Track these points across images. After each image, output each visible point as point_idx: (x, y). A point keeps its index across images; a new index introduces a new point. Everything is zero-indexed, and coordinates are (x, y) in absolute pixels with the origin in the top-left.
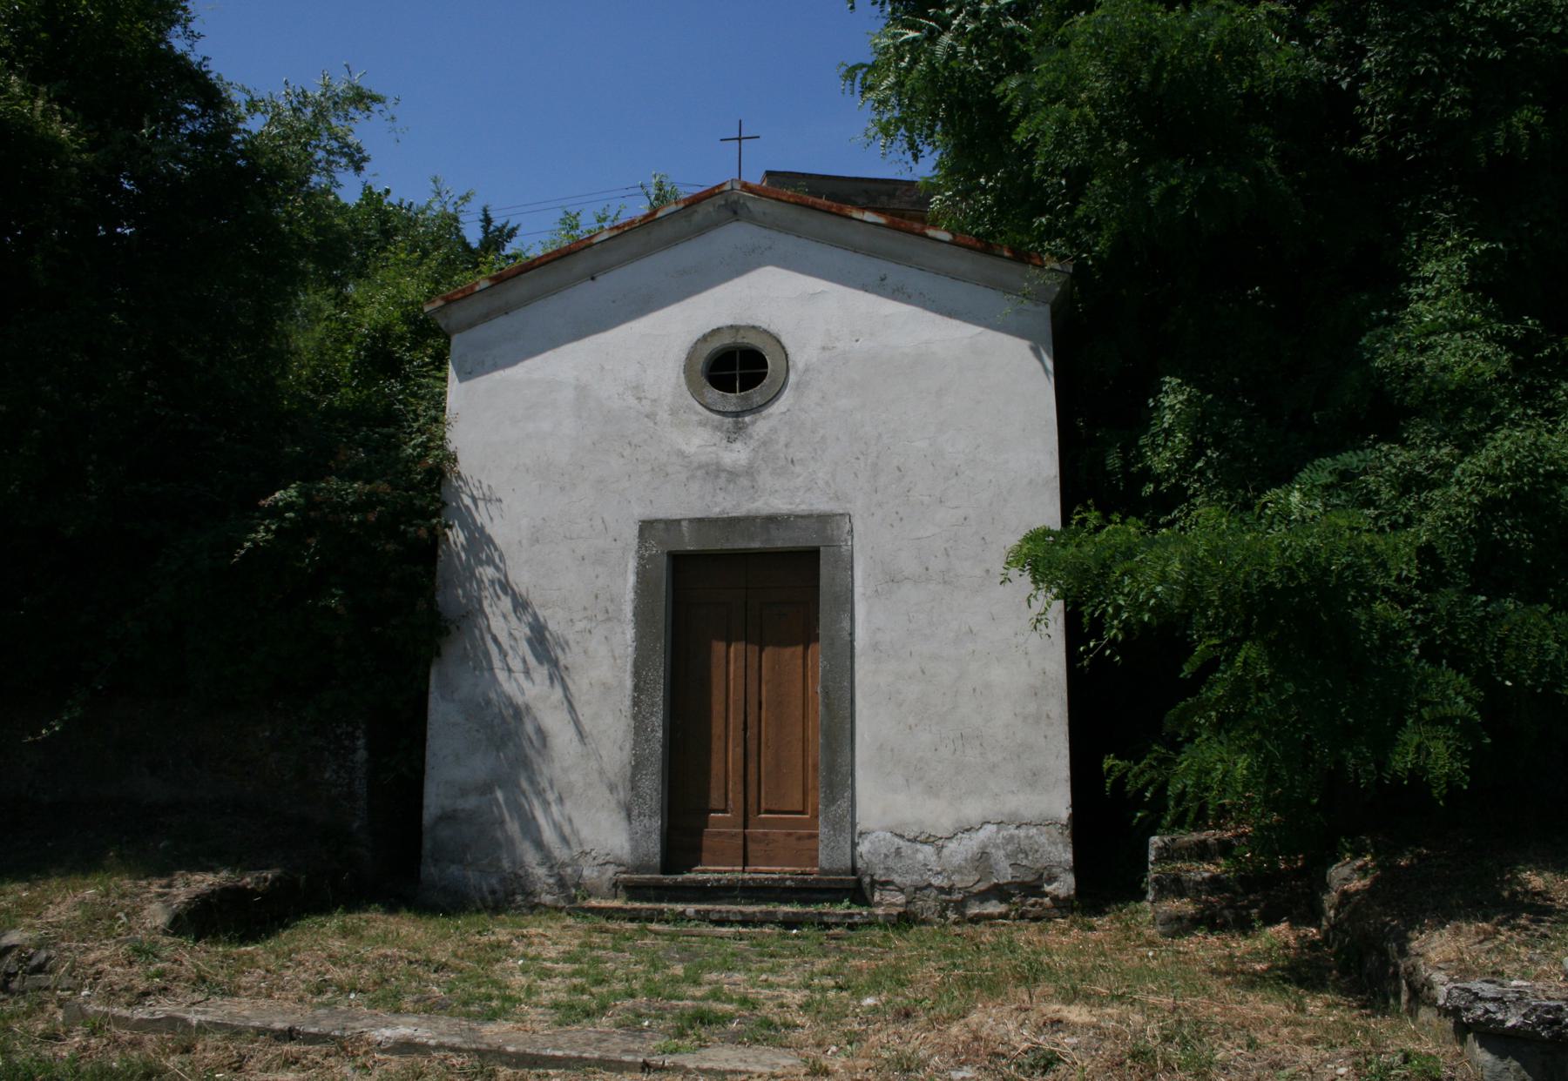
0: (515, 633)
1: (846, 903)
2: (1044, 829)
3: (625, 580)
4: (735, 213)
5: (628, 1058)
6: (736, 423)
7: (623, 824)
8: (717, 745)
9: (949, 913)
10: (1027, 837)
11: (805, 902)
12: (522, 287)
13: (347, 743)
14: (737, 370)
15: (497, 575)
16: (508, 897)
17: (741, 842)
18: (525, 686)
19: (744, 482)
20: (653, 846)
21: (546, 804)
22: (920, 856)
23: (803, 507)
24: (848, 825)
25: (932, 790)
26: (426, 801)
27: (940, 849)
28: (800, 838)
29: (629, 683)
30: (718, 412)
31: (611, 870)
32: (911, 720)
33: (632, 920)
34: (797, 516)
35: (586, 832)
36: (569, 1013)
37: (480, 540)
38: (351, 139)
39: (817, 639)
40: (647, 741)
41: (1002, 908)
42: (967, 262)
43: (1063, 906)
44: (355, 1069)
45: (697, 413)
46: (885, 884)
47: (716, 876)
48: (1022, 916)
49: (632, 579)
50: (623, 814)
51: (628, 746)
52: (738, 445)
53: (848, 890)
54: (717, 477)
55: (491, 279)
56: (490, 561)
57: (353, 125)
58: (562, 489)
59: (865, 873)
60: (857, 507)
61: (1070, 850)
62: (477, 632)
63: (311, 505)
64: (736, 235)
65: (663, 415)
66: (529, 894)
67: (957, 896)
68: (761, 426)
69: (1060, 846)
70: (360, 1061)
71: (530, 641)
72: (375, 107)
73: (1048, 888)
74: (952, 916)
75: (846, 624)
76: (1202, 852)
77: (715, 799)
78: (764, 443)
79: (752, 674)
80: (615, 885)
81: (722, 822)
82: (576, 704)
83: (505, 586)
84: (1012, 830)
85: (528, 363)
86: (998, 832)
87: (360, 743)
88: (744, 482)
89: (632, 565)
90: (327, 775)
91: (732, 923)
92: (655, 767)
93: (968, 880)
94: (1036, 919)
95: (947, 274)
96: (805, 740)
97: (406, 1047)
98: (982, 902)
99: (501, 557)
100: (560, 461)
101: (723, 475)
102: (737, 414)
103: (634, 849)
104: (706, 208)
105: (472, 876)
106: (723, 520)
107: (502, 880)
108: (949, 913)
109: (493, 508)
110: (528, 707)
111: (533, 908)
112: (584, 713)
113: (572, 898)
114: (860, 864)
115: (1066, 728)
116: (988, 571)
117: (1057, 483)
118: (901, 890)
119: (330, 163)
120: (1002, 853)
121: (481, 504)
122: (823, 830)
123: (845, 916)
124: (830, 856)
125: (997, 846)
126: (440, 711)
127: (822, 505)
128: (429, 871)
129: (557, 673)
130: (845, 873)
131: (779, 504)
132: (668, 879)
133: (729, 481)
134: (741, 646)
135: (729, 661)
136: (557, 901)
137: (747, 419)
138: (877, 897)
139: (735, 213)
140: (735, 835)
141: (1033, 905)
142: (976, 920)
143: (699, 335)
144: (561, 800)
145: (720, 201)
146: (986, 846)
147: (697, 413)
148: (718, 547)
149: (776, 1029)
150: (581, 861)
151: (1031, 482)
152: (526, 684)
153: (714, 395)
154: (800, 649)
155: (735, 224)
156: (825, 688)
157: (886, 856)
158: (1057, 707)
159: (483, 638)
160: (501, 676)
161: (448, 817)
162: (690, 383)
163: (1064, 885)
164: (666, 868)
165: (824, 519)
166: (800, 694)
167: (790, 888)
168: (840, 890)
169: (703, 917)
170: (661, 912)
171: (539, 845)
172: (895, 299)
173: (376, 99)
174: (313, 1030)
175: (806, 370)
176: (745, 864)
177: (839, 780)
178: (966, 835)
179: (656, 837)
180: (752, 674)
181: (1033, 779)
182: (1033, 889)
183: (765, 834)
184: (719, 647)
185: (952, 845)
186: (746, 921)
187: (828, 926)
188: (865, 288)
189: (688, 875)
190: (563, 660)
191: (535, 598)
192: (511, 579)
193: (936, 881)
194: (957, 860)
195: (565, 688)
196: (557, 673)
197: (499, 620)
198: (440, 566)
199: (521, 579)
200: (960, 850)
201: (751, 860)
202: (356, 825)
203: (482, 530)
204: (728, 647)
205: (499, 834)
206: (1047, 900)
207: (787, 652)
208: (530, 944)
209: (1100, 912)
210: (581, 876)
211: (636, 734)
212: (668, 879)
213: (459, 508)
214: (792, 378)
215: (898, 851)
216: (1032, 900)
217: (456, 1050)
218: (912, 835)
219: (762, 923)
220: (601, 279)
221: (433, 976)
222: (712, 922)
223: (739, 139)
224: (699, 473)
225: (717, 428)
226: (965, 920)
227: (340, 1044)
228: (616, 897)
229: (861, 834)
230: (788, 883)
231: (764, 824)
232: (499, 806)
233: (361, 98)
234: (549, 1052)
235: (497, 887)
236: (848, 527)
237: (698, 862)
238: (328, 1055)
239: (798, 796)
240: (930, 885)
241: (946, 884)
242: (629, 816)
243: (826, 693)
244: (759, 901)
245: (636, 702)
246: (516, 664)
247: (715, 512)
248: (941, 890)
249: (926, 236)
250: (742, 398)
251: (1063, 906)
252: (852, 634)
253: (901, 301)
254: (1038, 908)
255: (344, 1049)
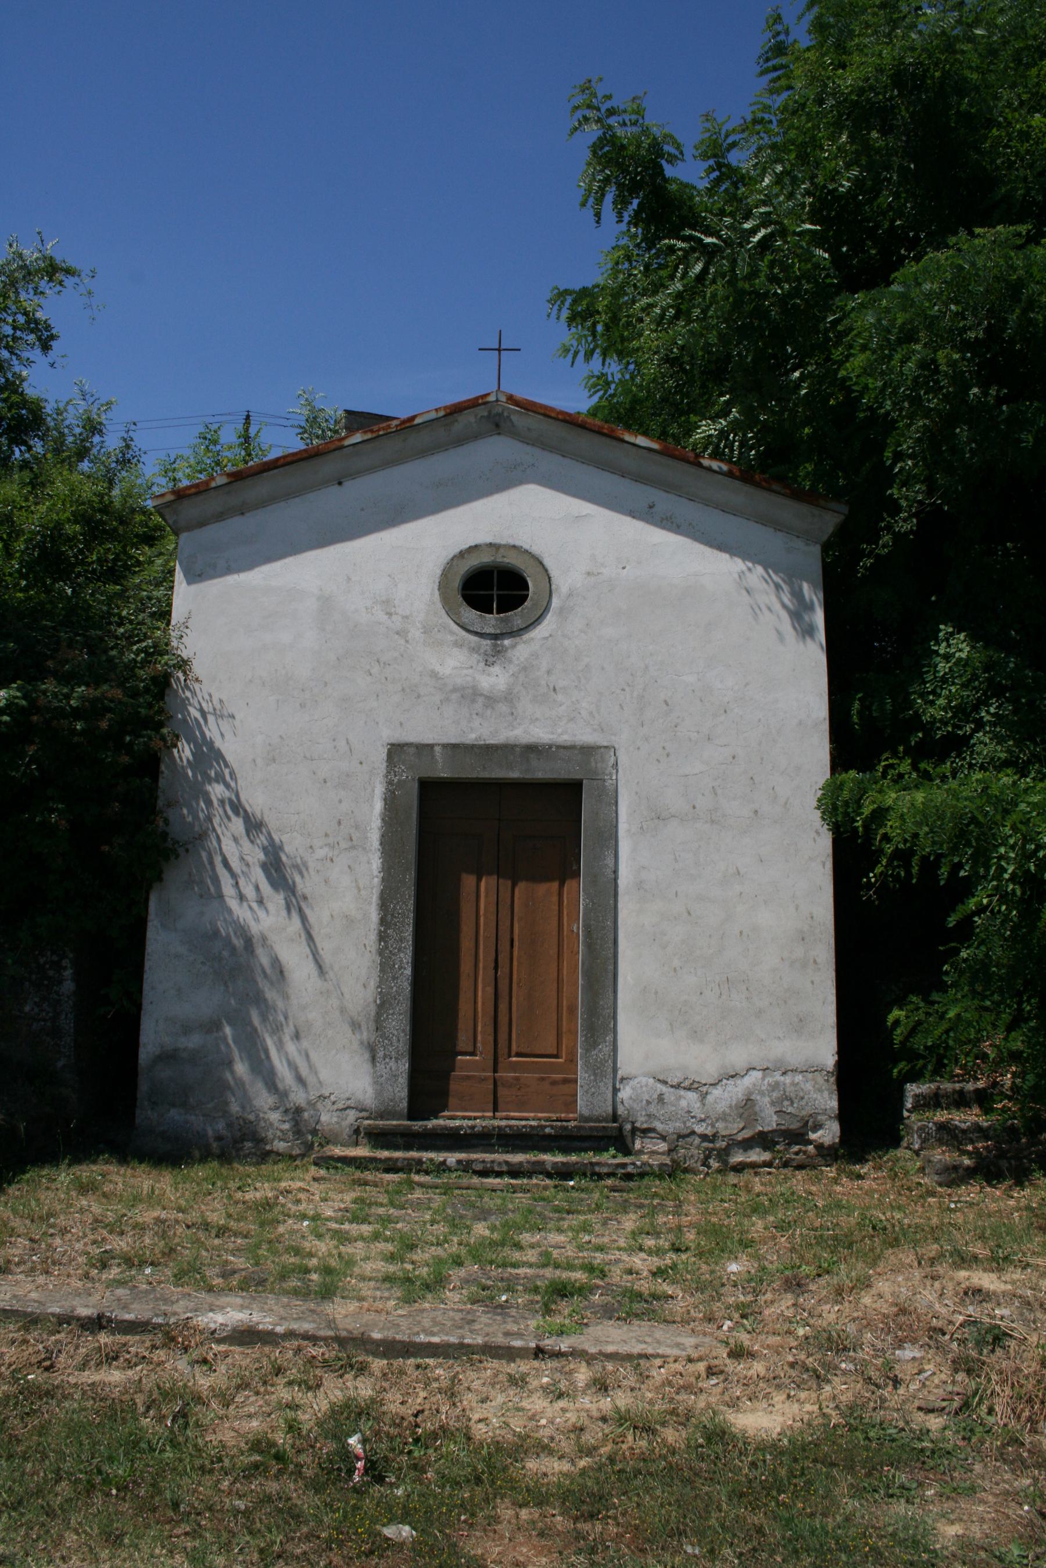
0: (248, 858)
1: (612, 1151)
2: (810, 1076)
3: (372, 806)
4: (497, 425)
5: (517, 1343)
6: (495, 646)
7: (367, 1067)
8: (465, 984)
9: (711, 1161)
10: (793, 1084)
11: (565, 1151)
12: (261, 487)
13: (51, 973)
14: (495, 590)
15: (227, 794)
16: (240, 1145)
17: (491, 1087)
18: (267, 920)
19: (503, 708)
20: (400, 1091)
21: (280, 1045)
22: (683, 1103)
23: (565, 737)
24: (608, 1069)
25: (696, 1035)
26: (143, 1039)
27: (704, 1096)
28: (554, 1083)
29: (374, 916)
30: (476, 634)
31: (352, 1115)
32: (676, 963)
33: (387, 1171)
34: (558, 747)
35: (324, 1074)
36: (414, 1289)
37: (209, 756)
38: (39, 315)
39: (577, 874)
40: (394, 978)
41: (766, 1156)
42: (739, 494)
43: (828, 1154)
44: (193, 1363)
45: (452, 633)
46: (645, 1131)
47: (470, 1123)
48: (786, 1165)
49: (378, 806)
50: (367, 1055)
51: (373, 984)
52: (496, 669)
53: (609, 1137)
54: (473, 701)
55: (229, 475)
56: (220, 778)
57: (42, 301)
58: (302, 706)
59: (626, 1120)
60: (622, 740)
61: (835, 1097)
62: (204, 854)
63: (34, 706)
64: (498, 448)
65: (416, 633)
66: (259, 1141)
67: (721, 1144)
68: (521, 650)
69: (826, 1094)
70: (195, 1354)
71: (264, 866)
72: (69, 281)
73: (813, 1136)
74: (715, 1164)
75: (610, 861)
76: (960, 1101)
77: (463, 1041)
78: (525, 669)
79: (504, 912)
80: (357, 1131)
81: (470, 1065)
82: (314, 934)
83: (237, 807)
84: (777, 1077)
85: (266, 569)
86: (763, 1079)
87: (68, 973)
88: (503, 708)
89: (379, 789)
90: (27, 1008)
91: (499, 1174)
92: (402, 1007)
93: (732, 1128)
94: (800, 1167)
95: (717, 507)
96: (559, 980)
97: (246, 1336)
98: (745, 1150)
99: (232, 774)
100: (302, 680)
101: (481, 700)
102: (495, 637)
103: (379, 1094)
104: (468, 418)
105: (195, 1120)
106: (480, 747)
107: (230, 1125)
108: (711, 1161)
109: (225, 725)
110: (264, 939)
111: (264, 1156)
112: (325, 947)
113: (309, 1144)
114: (621, 1110)
115: (832, 975)
116: (756, 812)
117: (826, 726)
118: (663, 1138)
119: (15, 339)
120: (767, 1099)
121: (211, 718)
122: (582, 1075)
123: (618, 1165)
124: (589, 1102)
125: (762, 1093)
126: (159, 940)
127: (585, 736)
128: (145, 1115)
129: (296, 904)
130: (605, 1120)
131: (540, 734)
132: (417, 1125)
133: (486, 706)
134: (493, 880)
135: (480, 895)
136: (291, 1148)
137: (507, 642)
138: (638, 1145)
139: (497, 425)
140: (485, 1079)
141: (797, 1153)
142: (739, 1168)
143: (456, 551)
144: (297, 1036)
145: (482, 411)
146: (750, 1093)
147: (452, 633)
148: (474, 776)
149: (646, 1301)
150: (319, 1105)
151: (800, 723)
152: (261, 914)
153: (470, 615)
154: (555, 885)
155: (496, 438)
156: (587, 926)
157: (648, 1103)
158: (824, 952)
159: (211, 862)
160: (233, 904)
161: (168, 1056)
162: (445, 600)
163: (829, 1133)
164: (414, 1112)
165: (588, 751)
166: (555, 933)
167: (549, 1136)
168: (601, 1138)
169: (465, 1167)
170: (420, 1162)
171: (271, 1083)
172: (663, 528)
173: (69, 272)
174: (129, 1317)
175: (570, 595)
176: (495, 1109)
177: (601, 1024)
178: (731, 1082)
179: (403, 1081)
180: (504, 912)
181: (799, 1025)
182: (797, 1137)
183: (517, 1079)
184: (468, 881)
185: (716, 1092)
186: (515, 1172)
187: (600, 1177)
188: (632, 514)
189: (435, 1122)
190: (303, 885)
191: (272, 822)
192: (243, 798)
193: (700, 1129)
194: (722, 1107)
195: (304, 919)
196: (296, 904)
197: (231, 842)
198: (162, 782)
199: (255, 800)
200: (725, 1097)
201: (501, 1105)
202: (60, 1064)
203: (210, 744)
204: (479, 880)
205: (228, 1076)
206: (811, 1148)
207: (542, 888)
208: (298, 1201)
209: (862, 1160)
210: (318, 1122)
211: (382, 970)
212: (417, 1125)
213: (185, 720)
214: (555, 602)
215: (661, 1098)
216: (796, 1148)
217: (313, 1339)
218: (675, 1082)
219: (529, 1175)
220: (348, 484)
221: (217, 1242)
222: (475, 1172)
223: (499, 350)
224: (454, 696)
225: (474, 650)
226: (727, 1168)
227: (167, 1334)
228: (357, 1144)
229: (622, 1079)
230: (547, 1130)
231: (514, 1067)
232: (228, 1045)
233: (52, 270)
234: (422, 1338)
235: (224, 1132)
236: (612, 760)
237: (445, 1107)
238: (154, 1347)
239: (552, 1038)
240: (693, 1133)
241: (709, 1131)
242: (373, 1059)
243: (588, 933)
244: (524, 1149)
245: (382, 937)
246: (249, 891)
247: (470, 738)
248: (704, 1137)
249: (700, 465)
250: (502, 620)
251: (828, 1154)
252: (616, 872)
253: (669, 530)
254: (801, 1156)
255: (173, 1339)
